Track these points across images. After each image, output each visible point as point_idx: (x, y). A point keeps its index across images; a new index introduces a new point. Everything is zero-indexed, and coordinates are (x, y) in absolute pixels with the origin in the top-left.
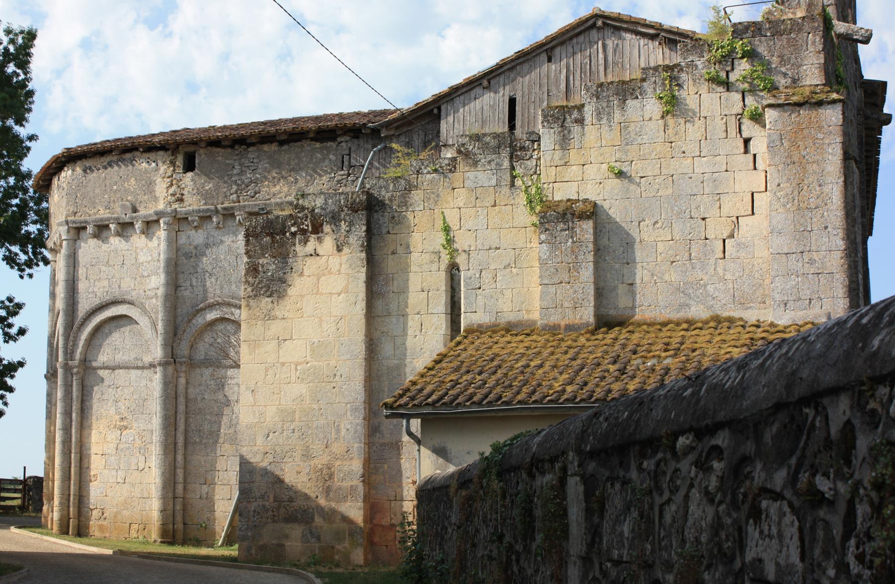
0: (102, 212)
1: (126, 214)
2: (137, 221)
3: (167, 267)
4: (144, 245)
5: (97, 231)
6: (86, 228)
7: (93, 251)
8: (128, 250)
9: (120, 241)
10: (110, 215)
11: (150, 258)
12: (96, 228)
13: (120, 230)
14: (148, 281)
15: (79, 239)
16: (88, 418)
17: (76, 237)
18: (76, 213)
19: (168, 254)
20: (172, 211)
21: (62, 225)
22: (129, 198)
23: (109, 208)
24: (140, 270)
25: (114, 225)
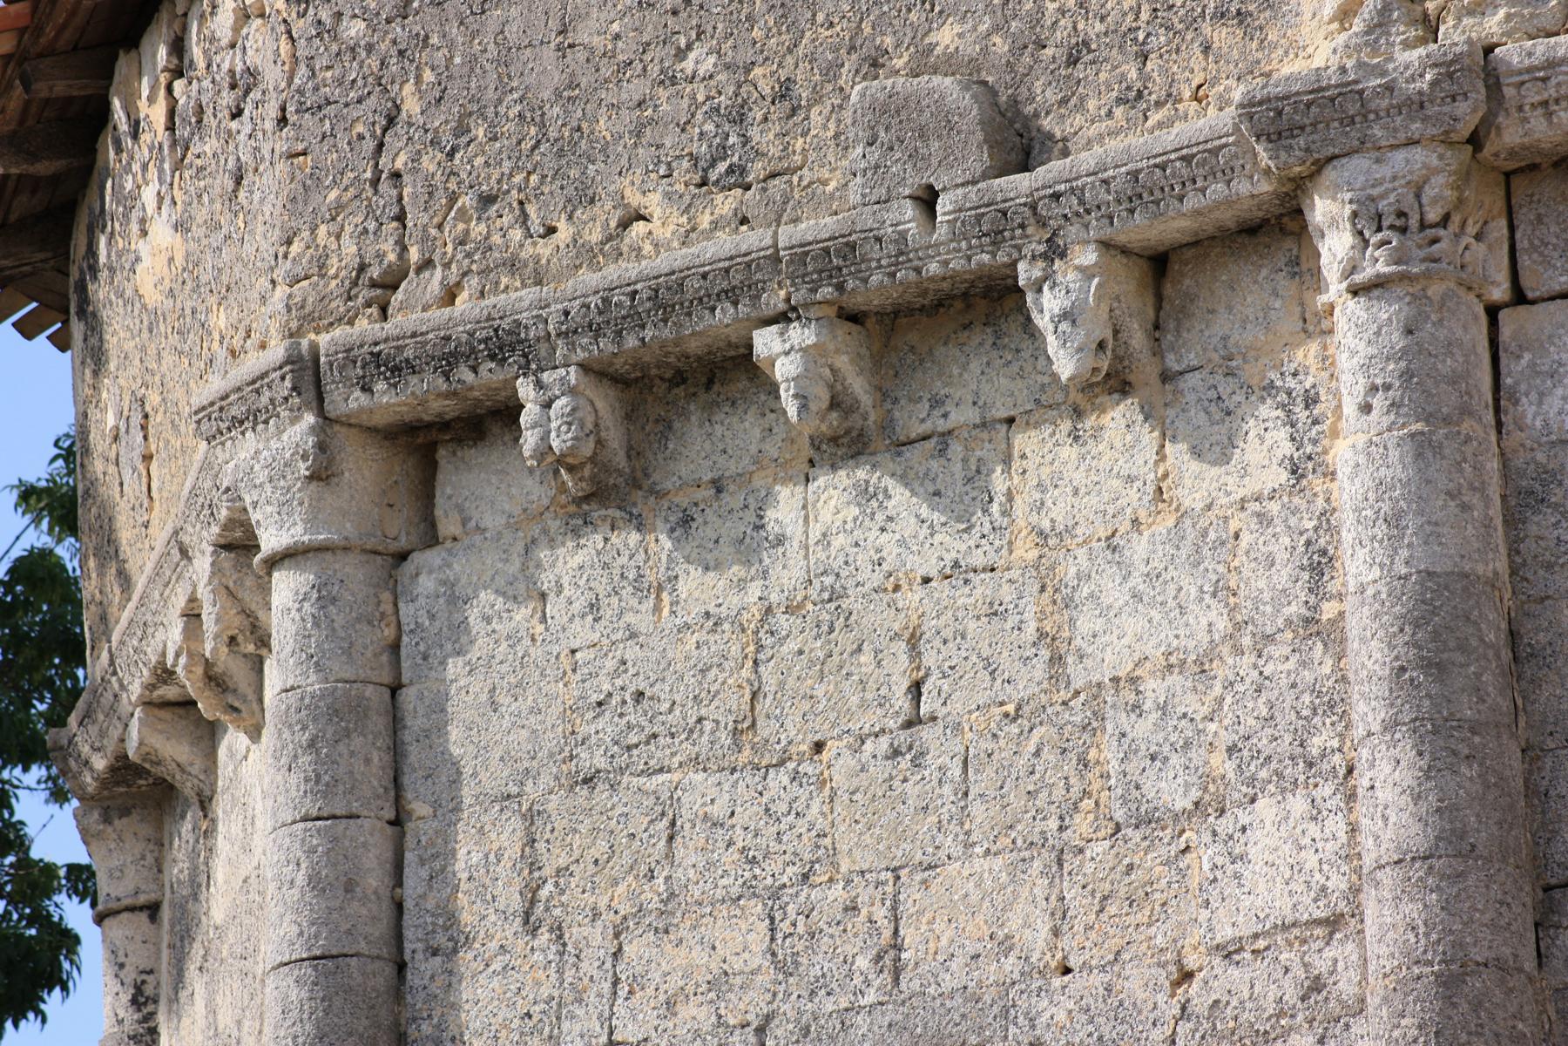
0: (664, 222)
1: (927, 200)
2: (1055, 251)
3: (1436, 667)
4: (1135, 499)
5: (615, 437)
6: (509, 412)
7: (583, 633)
8: (956, 571)
9: (866, 494)
10: (753, 239)
11: (1210, 619)
12: (604, 402)
13: (859, 386)
14: (1206, 857)
15: (432, 538)
16: (417, 499)
17: (400, 529)
18: (390, 283)
19: (1432, 532)
20: (1449, 70)
21: (253, 418)
22: (946, 37)
23: (738, 178)
24: (1109, 754)
25: (801, 335)
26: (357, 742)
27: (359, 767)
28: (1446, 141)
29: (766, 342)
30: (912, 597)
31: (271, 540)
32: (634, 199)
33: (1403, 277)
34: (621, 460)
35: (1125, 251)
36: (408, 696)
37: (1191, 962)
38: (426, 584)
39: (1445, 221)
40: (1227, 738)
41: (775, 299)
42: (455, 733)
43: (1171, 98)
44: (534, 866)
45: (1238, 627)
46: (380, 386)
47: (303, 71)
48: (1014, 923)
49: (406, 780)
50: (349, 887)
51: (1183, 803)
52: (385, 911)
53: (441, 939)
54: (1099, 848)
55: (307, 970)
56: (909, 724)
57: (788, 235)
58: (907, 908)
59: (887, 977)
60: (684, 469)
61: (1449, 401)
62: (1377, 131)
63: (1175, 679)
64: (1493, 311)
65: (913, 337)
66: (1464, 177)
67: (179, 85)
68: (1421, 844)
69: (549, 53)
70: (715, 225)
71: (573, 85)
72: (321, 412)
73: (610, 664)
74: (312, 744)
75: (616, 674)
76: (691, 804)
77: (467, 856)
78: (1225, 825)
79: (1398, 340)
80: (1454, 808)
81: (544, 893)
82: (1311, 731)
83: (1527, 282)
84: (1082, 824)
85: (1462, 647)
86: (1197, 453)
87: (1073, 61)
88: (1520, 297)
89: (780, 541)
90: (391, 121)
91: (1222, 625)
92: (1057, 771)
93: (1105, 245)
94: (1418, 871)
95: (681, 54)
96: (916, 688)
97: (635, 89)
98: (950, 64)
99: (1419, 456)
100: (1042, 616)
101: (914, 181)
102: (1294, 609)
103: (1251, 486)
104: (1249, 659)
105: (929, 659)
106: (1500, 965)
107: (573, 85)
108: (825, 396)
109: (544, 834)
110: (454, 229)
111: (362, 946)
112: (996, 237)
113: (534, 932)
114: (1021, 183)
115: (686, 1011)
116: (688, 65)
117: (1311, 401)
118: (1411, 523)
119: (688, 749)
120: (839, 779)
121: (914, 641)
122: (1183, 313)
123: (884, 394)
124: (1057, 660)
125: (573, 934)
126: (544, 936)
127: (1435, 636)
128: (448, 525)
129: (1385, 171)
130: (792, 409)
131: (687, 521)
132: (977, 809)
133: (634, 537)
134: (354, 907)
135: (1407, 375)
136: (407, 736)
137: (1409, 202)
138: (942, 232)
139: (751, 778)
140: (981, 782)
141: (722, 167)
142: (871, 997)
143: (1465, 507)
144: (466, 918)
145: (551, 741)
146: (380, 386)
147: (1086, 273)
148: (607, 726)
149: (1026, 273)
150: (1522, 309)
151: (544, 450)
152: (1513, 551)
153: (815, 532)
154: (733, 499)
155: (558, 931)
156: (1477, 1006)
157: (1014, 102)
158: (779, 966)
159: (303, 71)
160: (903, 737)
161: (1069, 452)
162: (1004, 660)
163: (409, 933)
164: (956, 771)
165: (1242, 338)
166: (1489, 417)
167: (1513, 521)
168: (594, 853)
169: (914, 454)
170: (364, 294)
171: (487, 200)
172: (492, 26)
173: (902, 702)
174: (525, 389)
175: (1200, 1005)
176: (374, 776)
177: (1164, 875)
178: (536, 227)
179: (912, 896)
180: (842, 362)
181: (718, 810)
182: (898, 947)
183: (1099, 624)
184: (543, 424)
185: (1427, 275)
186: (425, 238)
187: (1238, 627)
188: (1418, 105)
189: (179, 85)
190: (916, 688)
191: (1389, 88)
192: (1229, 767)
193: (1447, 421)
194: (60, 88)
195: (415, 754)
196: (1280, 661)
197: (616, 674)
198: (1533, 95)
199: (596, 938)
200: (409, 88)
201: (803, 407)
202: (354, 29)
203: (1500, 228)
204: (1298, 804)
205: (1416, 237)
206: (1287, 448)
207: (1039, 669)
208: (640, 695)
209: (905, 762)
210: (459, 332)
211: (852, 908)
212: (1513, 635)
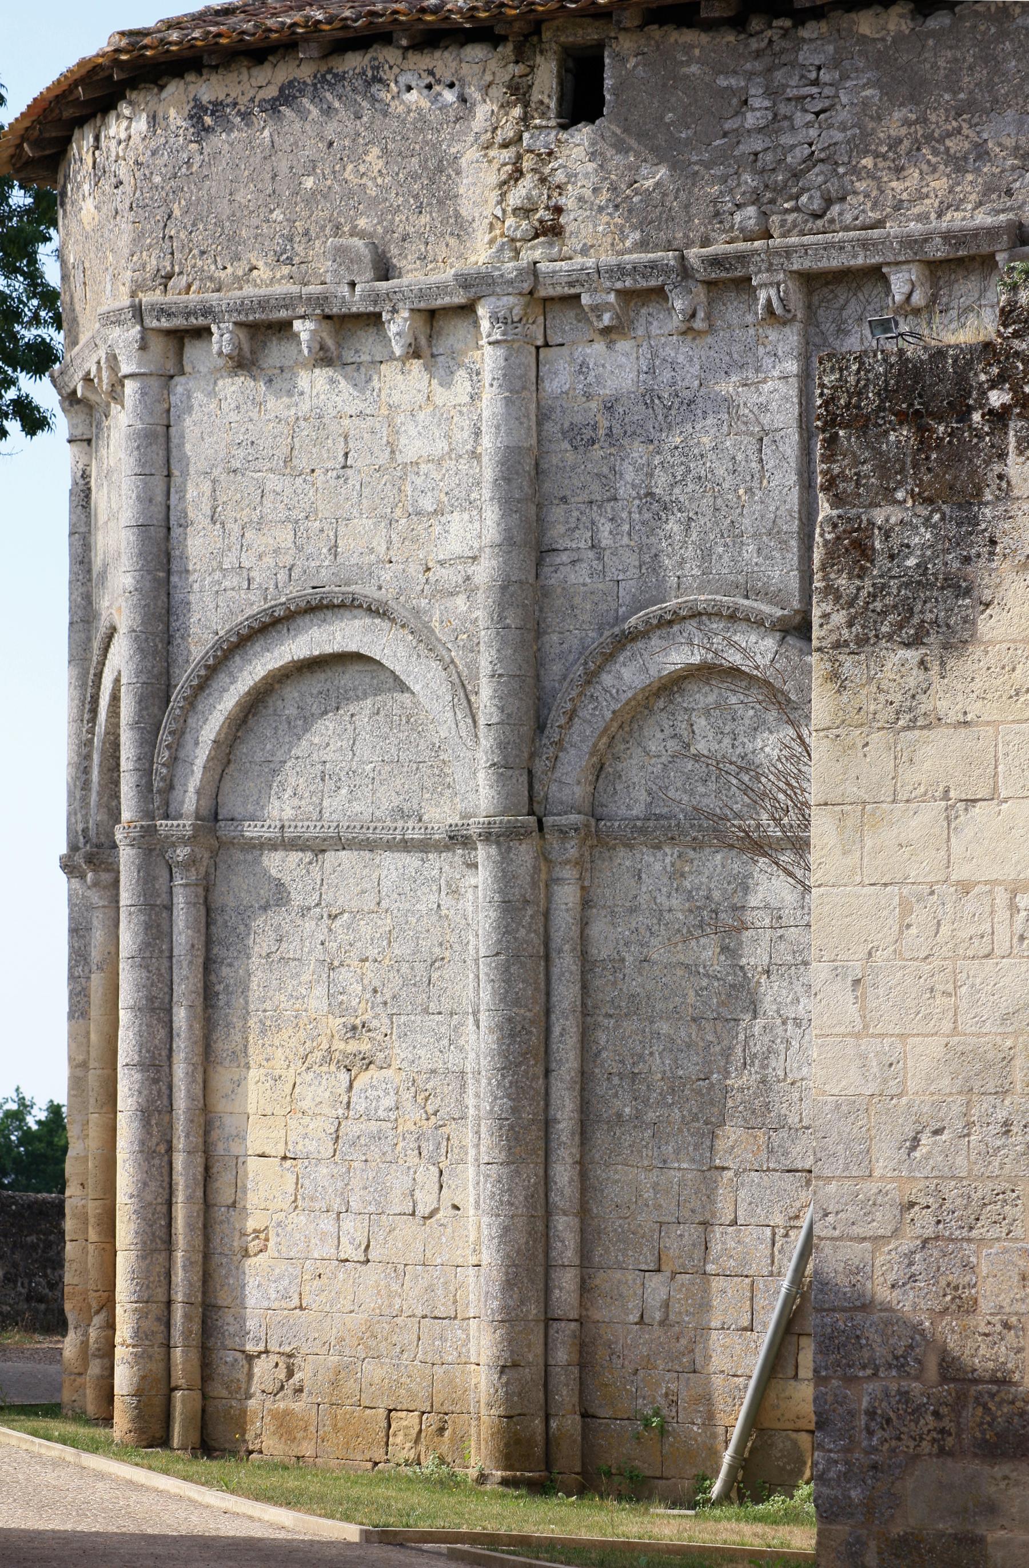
0: (263, 273)
1: (353, 285)
2: (394, 311)
3: (508, 480)
4: (421, 398)
5: (246, 347)
7: (233, 416)
9: (332, 381)
10: (294, 289)
11: (442, 446)
12: (242, 335)
13: (330, 343)
14: (437, 529)
15: (182, 373)
17: (171, 367)
18: (169, 277)
19: (509, 433)
20: (521, 271)
21: (118, 322)
22: (362, 223)
23: (290, 261)
24: (409, 489)
25: (309, 325)
26: (154, 447)
27: (155, 456)
28: (520, 294)
29: (297, 325)
30: (346, 422)
31: (125, 369)
32: (254, 262)
33: (505, 341)
34: (248, 355)
35: (419, 310)
36: (172, 430)
37: (430, 565)
38: (180, 389)
39: (520, 320)
40: (446, 489)
41: (301, 311)
42: (188, 447)
43: (435, 260)
44: (215, 500)
45: (451, 450)
46: (163, 320)
47: (138, 192)
48: (374, 544)
49: (172, 461)
50: (150, 501)
51: (431, 509)
52: (164, 509)
53: (182, 521)
54: (403, 521)
55: (135, 530)
56: (343, 467)
57: (306, 290)
58: (340, 533)
59: (332, 557)
60: (270, 361)
61: (518, 384)
62: (498, 290)
63: (430, 465)
64: (538, 348)
65: (350, 326)
66: (527, 305)
67: (97, 153)
68: (498, 541)
69: (226, 201)
70: (282, 277)
71: (234, 215)
72: (142, 326)
73: (243, 430)
74: (138, 447)
75: (245, 434)
76: (269, 486)
77: (191, 493)
78: (443, 519)
79: (503, 363)
80: (510, 529)
81: (219, 509)
82: (471, 491)
83: (549, 339)
84: (398, 512)
85: (517, 473)
86: (441, 385)
87: (404, 240)
88: (547, 345)
89: (302, 394)
90: (170, 217)
91: (446, 448)
92: (390, 492)
93: (412, 310)
94: (497, 550)
95: (271, 211)
96: (346, 455)
97: (255, 222)
98: (361, 234)
99: (507, 405)
100: (388, 436)
101: (348, 278)
102: (469, 447)
103: (458, 401)
104: (454, 462)
105: (351, 445)
106: (521, 582)
107: (234, 215)
108: (318, 347)
109: (219, 489)
110: (190, 262)
111: (155, 522)
112: (375, 303)
113: (215, 523)
114: (383, 285)
115: (265, 559)
116: (274, 216)
117: (478, 374)
118: (503, 429)
119: (269, 465)
120: (319, 484)
121: (346, 437)
122: (439, 334)
123: (339, 345)
124: (393, 452)
125: (228, 526)
126: (218, 526)
127: (508, 469)
128: (188, 368)
129: (500, 303)
130: (306, 351)
131: (271, 381)
132: (364, 501)
133: (252, 383)
134: (152, 508)
135: (505, 375)
136: (172, 445)
137: (508, 315)
138: (357, 298)
139: (288, 478)
140: (366, 491)
141: (285, 256)
142: (327, 563)
143: (521, 423)
144: (190, 514)
145: (222, 455)
146: (163, 320)
147: (405, 320)
148: (241, 453)
149: (385, 316)
150: (547, 349)
151: (220, 353)
152: (539, 434)
153: (314, 393)
154: (287, 375)
155: (223, 524)
156: (512, 596)
157: (384, 252)
158: (297, 548)
159: (138, 192)
160: (341, 472)
161: (400, 377)
162: (376, 450)
163: (172, 518)
164: (358, 487)
165: (459, 346)
166: (534, 388)
167: (539, 424)
168: (235, 498)
169: (349, 368)
170: (159, 281)
171: (203, 253)
172: (206, 188)
173: (341, 459)
174: (214, 328)
175: (432, 580)
176: (160, 460)
177: (424, 534)
178: (220, 266)
179: (342, 530)
180: (324, 335)
181: (278, 489)
182: (336, 546)
183: (407, 442)
184: (220, 342)
185: (513, 340)
186: (181, 263)
187: (451, 450)
188: (511, 282)
189: (97, 153)
190: (346, 455)
191: (502, 276)
192: (446, 499)
193: (517, 392)
194: (54, 134)
195: (174, 452)
196: (463, 466)
197: (245, 434)
198: (548, 281)
199: (236, 528)
200: (176, 205)
201: (310, 351)
202: (157, 179)
203: (541, 319)
204: (466, 516)
205: (510, 326)
206: (470, 389)
207: (387, 454)
208: (253, 443)
209: (342, 481)
210: (191, 305)
211: (322, 531)
212: (537, 465)
